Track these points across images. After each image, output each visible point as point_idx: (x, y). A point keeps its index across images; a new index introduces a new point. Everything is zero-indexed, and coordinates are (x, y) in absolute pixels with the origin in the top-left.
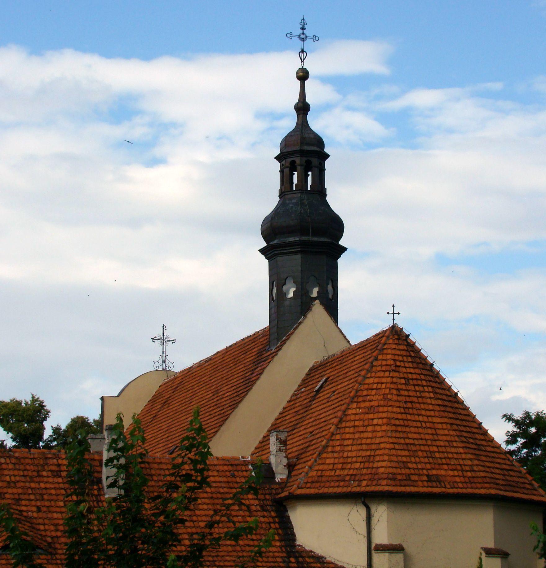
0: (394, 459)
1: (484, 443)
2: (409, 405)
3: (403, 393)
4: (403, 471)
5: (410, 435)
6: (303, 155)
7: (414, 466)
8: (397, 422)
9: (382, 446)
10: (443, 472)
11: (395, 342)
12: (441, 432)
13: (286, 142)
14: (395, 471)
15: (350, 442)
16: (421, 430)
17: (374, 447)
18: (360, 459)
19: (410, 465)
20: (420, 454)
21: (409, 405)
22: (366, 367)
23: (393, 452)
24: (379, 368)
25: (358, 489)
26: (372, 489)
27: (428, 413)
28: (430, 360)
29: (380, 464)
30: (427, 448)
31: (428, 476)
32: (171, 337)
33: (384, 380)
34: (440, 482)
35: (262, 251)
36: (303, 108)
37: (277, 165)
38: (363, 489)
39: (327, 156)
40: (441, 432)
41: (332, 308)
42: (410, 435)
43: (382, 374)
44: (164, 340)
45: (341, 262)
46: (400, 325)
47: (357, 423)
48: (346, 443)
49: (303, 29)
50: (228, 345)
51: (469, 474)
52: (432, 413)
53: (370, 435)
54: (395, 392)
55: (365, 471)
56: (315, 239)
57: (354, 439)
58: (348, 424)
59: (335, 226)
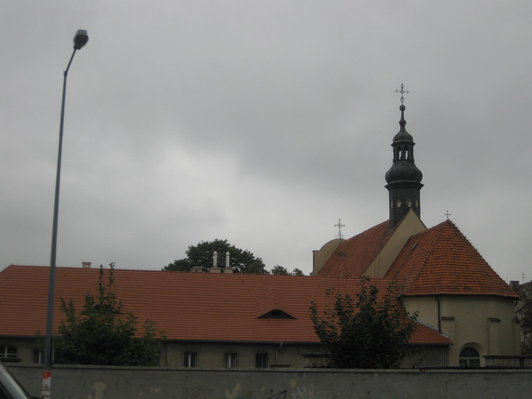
0: (450, 279)
1: (489, 272)
2: (456, 255)
3: (453, 250)
4: (454, 285)
5: (457, 269)
6: (403, 144)
7: (459, 282)
8: (451, 263)
9: (445, 274)
10: (471, 285)
11: (448, 229)
12: (470, 267)
13: (396, 138)
14: (450, 285)
15: (430, 272)
16: (461, 267)
17: (441, 274)
18: (435, 280)
19: (457, 282)
20: (461, 277)
21: (456, 255)
22: (436, 238)
23: (449, 276)
24: (442, 239)
25: (434, 293)
26: (440, 293)
27: (464, 259)
28: (464, 235)
29: (443, 282)
30: (464, 274)
31: (465, 287)
32: (343, 224)
33: (444, 245)
34: (470, 289)
35: (386, 187)
36: (403, 123)
37: (392, 148)
38: (436, 293)
39: (414, 144)
40: (470, 267)
41: (417, 211)
42: (457, 269)
43: (443, 242)
44: (340, 226)
45: (422, 191)
46: (451, 220)
47: (433, 264)
48: (428, 272)
49: (402, 88)
50: (370, 228)
51: (483, 286)
52: (466, 259)
53: (439, 269)
54: (449, 250)
55: (437, 285)
56: (410, 181)
57: (431, 271)
58: (429, 264)
59: (418, 175)
